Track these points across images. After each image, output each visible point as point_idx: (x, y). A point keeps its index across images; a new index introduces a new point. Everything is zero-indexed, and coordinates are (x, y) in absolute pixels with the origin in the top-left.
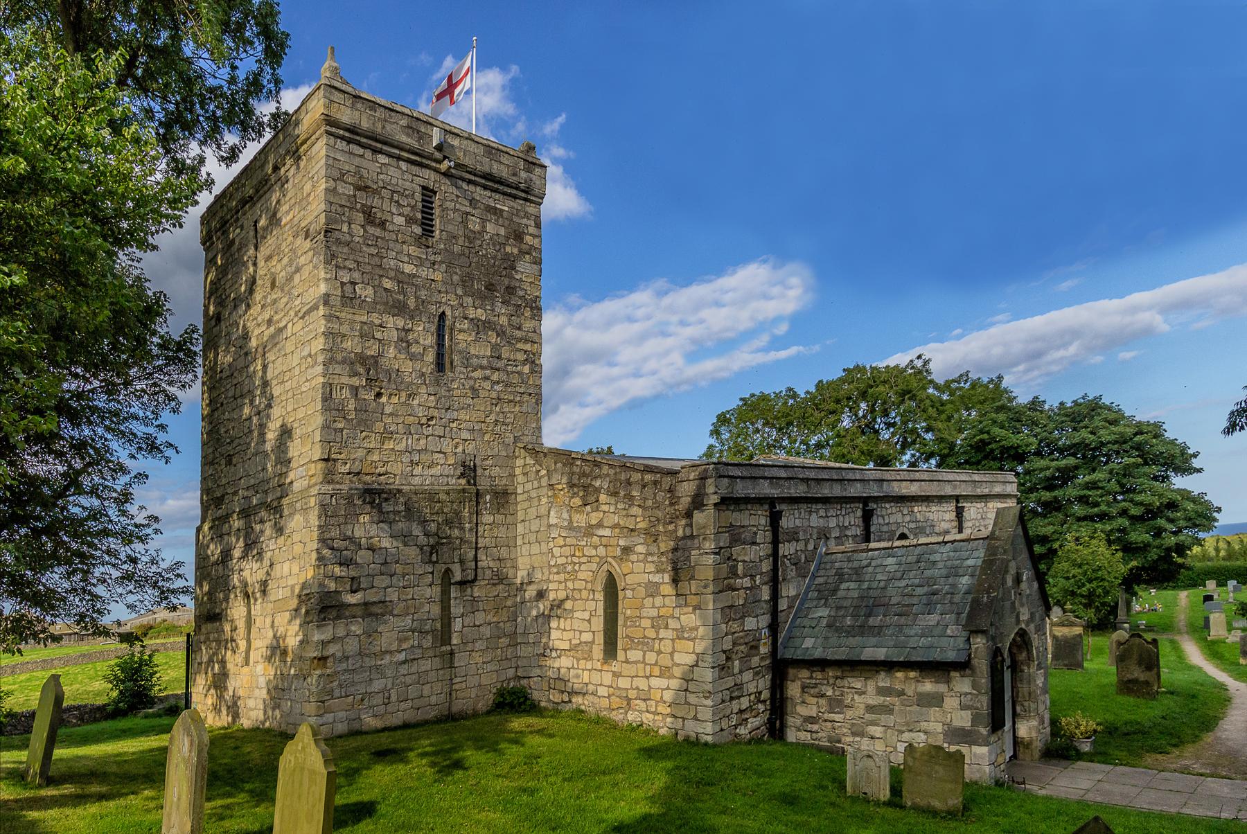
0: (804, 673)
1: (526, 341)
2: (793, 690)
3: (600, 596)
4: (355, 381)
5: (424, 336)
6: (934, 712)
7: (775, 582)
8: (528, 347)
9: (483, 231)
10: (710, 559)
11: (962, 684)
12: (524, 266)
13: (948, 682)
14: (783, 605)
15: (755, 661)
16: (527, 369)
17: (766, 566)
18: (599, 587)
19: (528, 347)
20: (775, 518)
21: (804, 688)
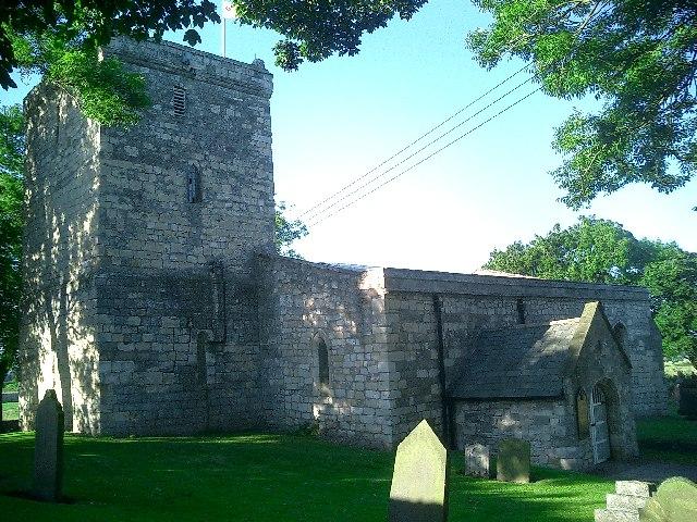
0: (466, 407)
1: (262, 184)
2: (460, 419)
3: (316, 355)
4: (126, 207)
5: (178, 179)
6: (545, 428)
7: (440, 349)
8: (262, 188)
9: (222, 114)
10: (384, 329)
11: (560, 410)
12: (257, 137)
13: (552, 408)
14: (448, 363)
15: (428, 398)
16: (261, 203)
17: (432, 337)
18: (316, 348)
19: (262, 188)
20: (437, 306)
21: (467, 417)
